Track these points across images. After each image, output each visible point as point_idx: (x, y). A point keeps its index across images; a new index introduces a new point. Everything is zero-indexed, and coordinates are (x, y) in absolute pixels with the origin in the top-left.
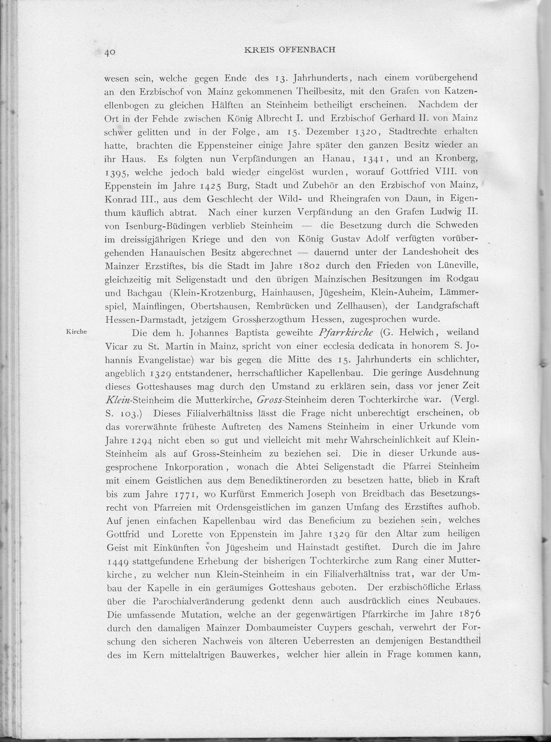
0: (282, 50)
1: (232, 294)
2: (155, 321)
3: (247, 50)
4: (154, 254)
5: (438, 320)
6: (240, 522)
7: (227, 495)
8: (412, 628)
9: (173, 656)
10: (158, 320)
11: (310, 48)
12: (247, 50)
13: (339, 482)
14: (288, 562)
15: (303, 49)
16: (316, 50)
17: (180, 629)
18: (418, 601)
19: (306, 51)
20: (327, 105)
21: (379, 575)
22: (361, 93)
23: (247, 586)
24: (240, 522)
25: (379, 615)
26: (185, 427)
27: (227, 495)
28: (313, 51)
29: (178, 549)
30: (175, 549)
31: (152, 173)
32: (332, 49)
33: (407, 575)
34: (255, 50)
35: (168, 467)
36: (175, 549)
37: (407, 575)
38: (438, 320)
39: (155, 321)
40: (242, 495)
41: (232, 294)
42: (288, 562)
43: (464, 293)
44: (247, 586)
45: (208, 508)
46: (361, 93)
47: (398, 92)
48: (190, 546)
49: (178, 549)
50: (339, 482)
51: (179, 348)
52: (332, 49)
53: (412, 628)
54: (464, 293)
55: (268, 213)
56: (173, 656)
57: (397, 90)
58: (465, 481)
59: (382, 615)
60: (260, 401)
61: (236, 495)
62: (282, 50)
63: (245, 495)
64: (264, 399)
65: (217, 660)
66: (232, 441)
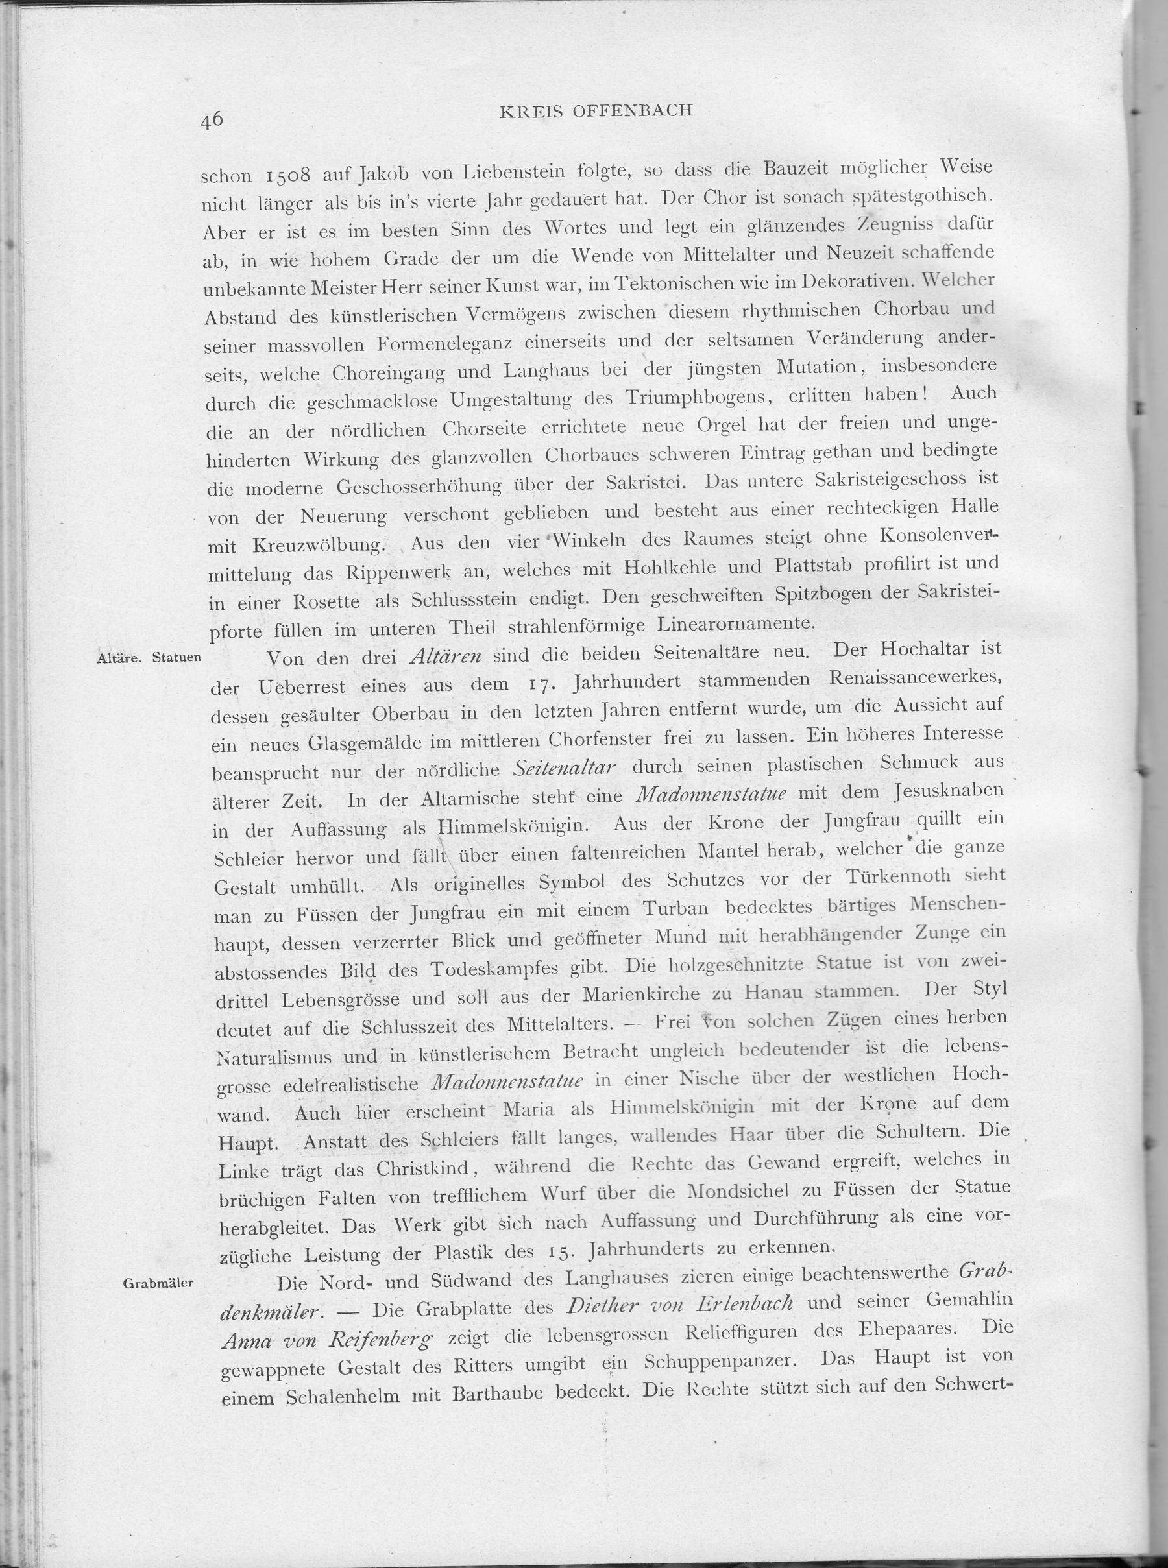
3: (505, 113)
7: (500, 288)
11: (639, 108)
12: (505, 113)
15: (623, 110)
16: (652, 110)
19: (630, 113)
20: (839, 453)
26: (845, 424)
27: (500, 288)
28: (646, 113)
31: (948, 706)
32: (686, 110)
38: (811, 625)
40: (981, 226)
48: (743, 591)
52: (686, 110)
62: (579, 111)
63: (872, 879)
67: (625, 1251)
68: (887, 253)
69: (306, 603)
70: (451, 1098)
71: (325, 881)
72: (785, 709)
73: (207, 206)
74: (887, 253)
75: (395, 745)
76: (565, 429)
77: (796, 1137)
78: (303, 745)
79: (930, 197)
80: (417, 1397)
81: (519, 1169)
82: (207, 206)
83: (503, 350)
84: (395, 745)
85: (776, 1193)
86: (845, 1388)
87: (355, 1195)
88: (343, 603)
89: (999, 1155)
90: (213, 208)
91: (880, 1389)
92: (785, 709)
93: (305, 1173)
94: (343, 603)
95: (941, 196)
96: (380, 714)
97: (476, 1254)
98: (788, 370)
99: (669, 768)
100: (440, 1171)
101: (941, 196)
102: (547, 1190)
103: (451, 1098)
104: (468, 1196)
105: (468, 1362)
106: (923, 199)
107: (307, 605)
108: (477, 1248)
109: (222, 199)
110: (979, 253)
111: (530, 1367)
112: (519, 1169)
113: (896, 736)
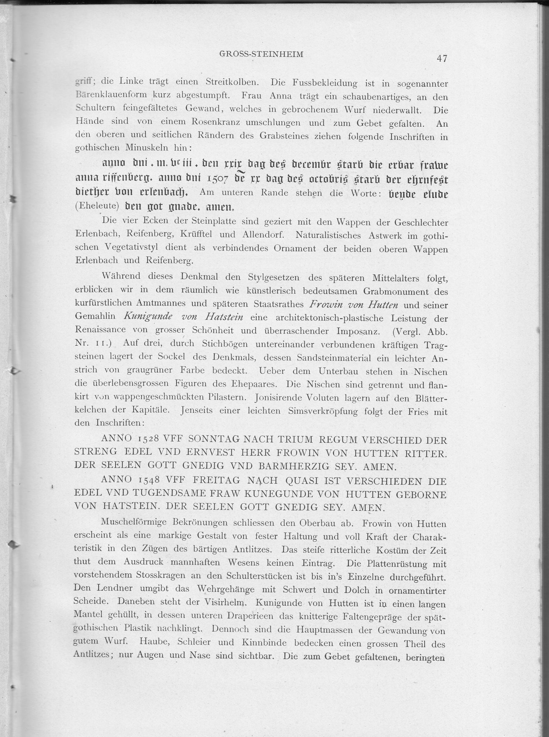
0: (391, 591)
4: (300, 631)
5: (168, 643)
6: (98, 262)
7: (263, 604)
9: (300, 223)
14: (325, 617)
17: (324, 236)
19: (275, 55)
22: (444, 413)
23: (154, 520)
24: (98, 262)
27: (263, 604)
29: (257, 292)
30: (254, 292)
34: (229, 53)
35: (210, 316)
36: (254, 292)
42: (325, 617)
44: (154, 520)
45: (444, 412)
46: (444, 413)
49: (257, 292)
54: (345, 292)
55: (157, 95)
56: (300, 223)
58: (373, 538)
61: (88, 304)
62: (391, 591)
66: (191, 384)
68: (230, 331)
69: (197, 122)
71: (266, 408)
73: (375, 111)
74: (230, 331)
77: (98, 384)
79: (82, 148)
81: (116, 277)
82: (375, 111)
87: (378, 656)
89: (271, 107)
90: (378, 111)
91: (386, 400)
93: (160, 82)
95: (88, 148)
97: (94, 549)
98: (131, 149)
100: (79, 398)
101: (88, 148)
102: (105, 274)
107: (198, 123)
108: (94, 546)
109: (247, 653)
110: (218, 136)
112: (116, 277)
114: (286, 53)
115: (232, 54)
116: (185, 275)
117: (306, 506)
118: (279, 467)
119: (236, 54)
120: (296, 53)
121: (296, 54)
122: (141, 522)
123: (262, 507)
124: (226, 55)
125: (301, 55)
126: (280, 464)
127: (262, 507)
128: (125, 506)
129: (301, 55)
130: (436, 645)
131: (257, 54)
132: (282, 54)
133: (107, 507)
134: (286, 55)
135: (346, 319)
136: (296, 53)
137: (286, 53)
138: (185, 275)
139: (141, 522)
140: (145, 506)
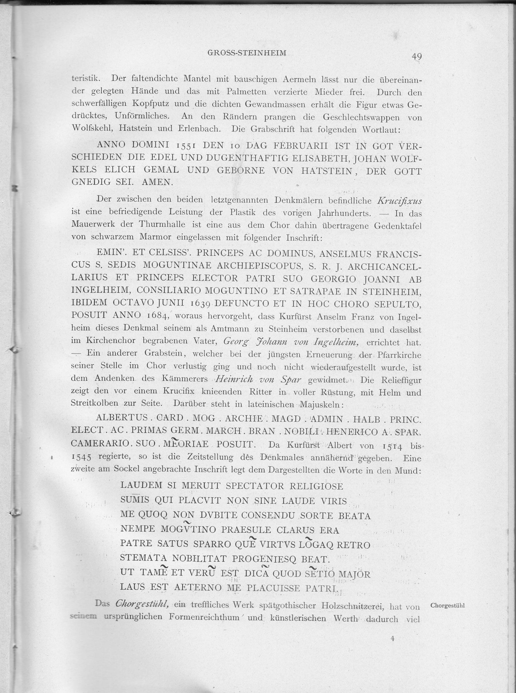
1: (274, 458)
2: (155, 238)
8: (96, 225)
10: (158, 237)
13: (261, 330)
14: (295, 213)
18: (414, 459)
21: (270, 406)
25: (393, 356)
26: (352, 92)
33: (399, 608)
34: (216, 53)
37: (399, 608)
39: (155, 238)
41: (274, 458)
42: (295, 213)
43: (160, 237)
47: (258, 130)
50: (261, 330)
51: (185, 404)
53: (96, 225)
54: (160, 237)
57: (257, 128)
59: (396, 356)
60: (226, 342)
64: (230, 340)
65: (358, 231)
67: (334, 214)
70: (329, 399)
72: (398, 369)
75: (308, 201)
76: (377, 343)
78: (405, 105)
80: (363, 393)
83: (370, 320)
84: (308, 201)
85: (415, 331)
86: (399, 93)
88: (254, 92)
92: (398, 369)
94: (254, 92)
96: (116, 302)
99: (396, 93)
103: (329, 399)
104: (207, 605)
105: (327, 390)
106: (280, 607)
111: (177, 105)
113: (397, 81)
114: (270, 52)
115: (219, 53)
116: (115, 77)
117: (100, 181)
118: (191, 431)
119: (223, 52)
120: (279, 52)
121: (279, 53)
122: (132, 116)
123: (415, 172)
124: (213, 54)
125: (284, 53)
126: (191, 429)
127: (415, 172)
128: (322, 171)
129: (284, 53)
130: (413, 214)
131: (243, 53)
132: (267, 53)
133: (305, 172)
134: (270, 53)
135: (147, 104)
136: (279, 52)
137: (270, 52)
138: (115, 77)
139: (132, 116)
140: (341, 171)
